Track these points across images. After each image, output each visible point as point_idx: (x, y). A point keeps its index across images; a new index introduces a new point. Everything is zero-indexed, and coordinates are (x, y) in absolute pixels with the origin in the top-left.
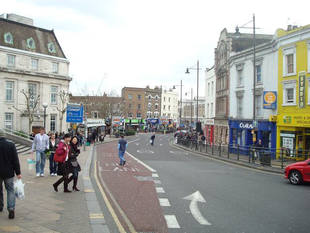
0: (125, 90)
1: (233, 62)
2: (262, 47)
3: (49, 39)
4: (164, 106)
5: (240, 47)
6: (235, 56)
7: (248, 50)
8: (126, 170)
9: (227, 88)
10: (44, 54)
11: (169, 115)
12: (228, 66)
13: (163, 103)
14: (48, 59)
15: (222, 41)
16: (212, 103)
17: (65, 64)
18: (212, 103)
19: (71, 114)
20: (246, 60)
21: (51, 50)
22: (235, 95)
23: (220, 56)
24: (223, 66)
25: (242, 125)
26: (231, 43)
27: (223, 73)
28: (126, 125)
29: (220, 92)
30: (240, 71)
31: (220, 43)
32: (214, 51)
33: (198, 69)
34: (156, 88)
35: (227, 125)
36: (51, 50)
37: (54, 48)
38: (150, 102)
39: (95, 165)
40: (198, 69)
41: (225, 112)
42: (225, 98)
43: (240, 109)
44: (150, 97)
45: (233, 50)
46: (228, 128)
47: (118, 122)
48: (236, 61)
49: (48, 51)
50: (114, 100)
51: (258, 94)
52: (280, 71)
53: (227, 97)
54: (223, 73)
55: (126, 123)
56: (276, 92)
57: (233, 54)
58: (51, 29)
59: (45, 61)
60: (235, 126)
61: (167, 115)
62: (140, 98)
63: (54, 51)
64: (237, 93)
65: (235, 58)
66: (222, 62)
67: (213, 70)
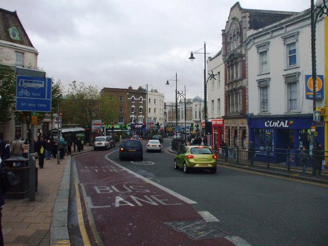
0: (106, 90)
1: (252, 43)
2: (291, 21)
3: (11, 22)
4: (150, 109)
5: (250, 26)
6: (253, 35)
7: (274, 25)
8: (140, 204)
9: (244, 76)
10: (5, 40)
11: (155, 119)
12: (243, 49)
13: (149, 106)
14: (10, 47)
15: (234, 19)
16: (213, 101)
17: (33, 55)
18: (213, 101)
19: (27, 93)
20: (272, 38)
21: (14, 36)
22: (256, 84)
23: (231, 38)
24: (235, 50)
25: (268, 124)
26: (248, 19)
27: (236, 59)
28: (107, 131)
29: (231, 83)
30: (263, 54)
31: (231, 21)
32: (221, 33)
33: (205, 53)
34: (140, 89)
35: (244, 123)
36: (14, 36)
37: (17, 34)
38: (133, 104)
39: (78, 194)
40: (205, 53)
41: (240, 109)
42: (241, 91)
43: (264, 102)
44: (133, 98)
45: (250, 28)
46: (247, 128)
47: (99, 126)
48: (256, 41)
49: (10, 37)
50: (93, 102)
51: (291, 81)
52: (287, 64)
53: (244, 90)
54: (236, 59)
55: (107, 130)
56: (323, 76)
57: (252, 32)
58: (13, 10)
59: (6, 50)
60: (257, 123)
61: (152, 119)
62: (124, 101)
63: (17, 38)
64: (260, 82)
65: (254, 37)
66: (234, 46)
67: (221, 57)
